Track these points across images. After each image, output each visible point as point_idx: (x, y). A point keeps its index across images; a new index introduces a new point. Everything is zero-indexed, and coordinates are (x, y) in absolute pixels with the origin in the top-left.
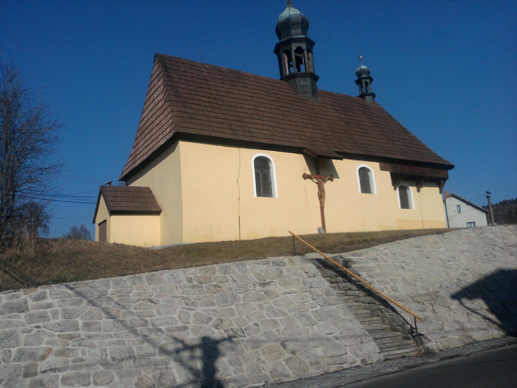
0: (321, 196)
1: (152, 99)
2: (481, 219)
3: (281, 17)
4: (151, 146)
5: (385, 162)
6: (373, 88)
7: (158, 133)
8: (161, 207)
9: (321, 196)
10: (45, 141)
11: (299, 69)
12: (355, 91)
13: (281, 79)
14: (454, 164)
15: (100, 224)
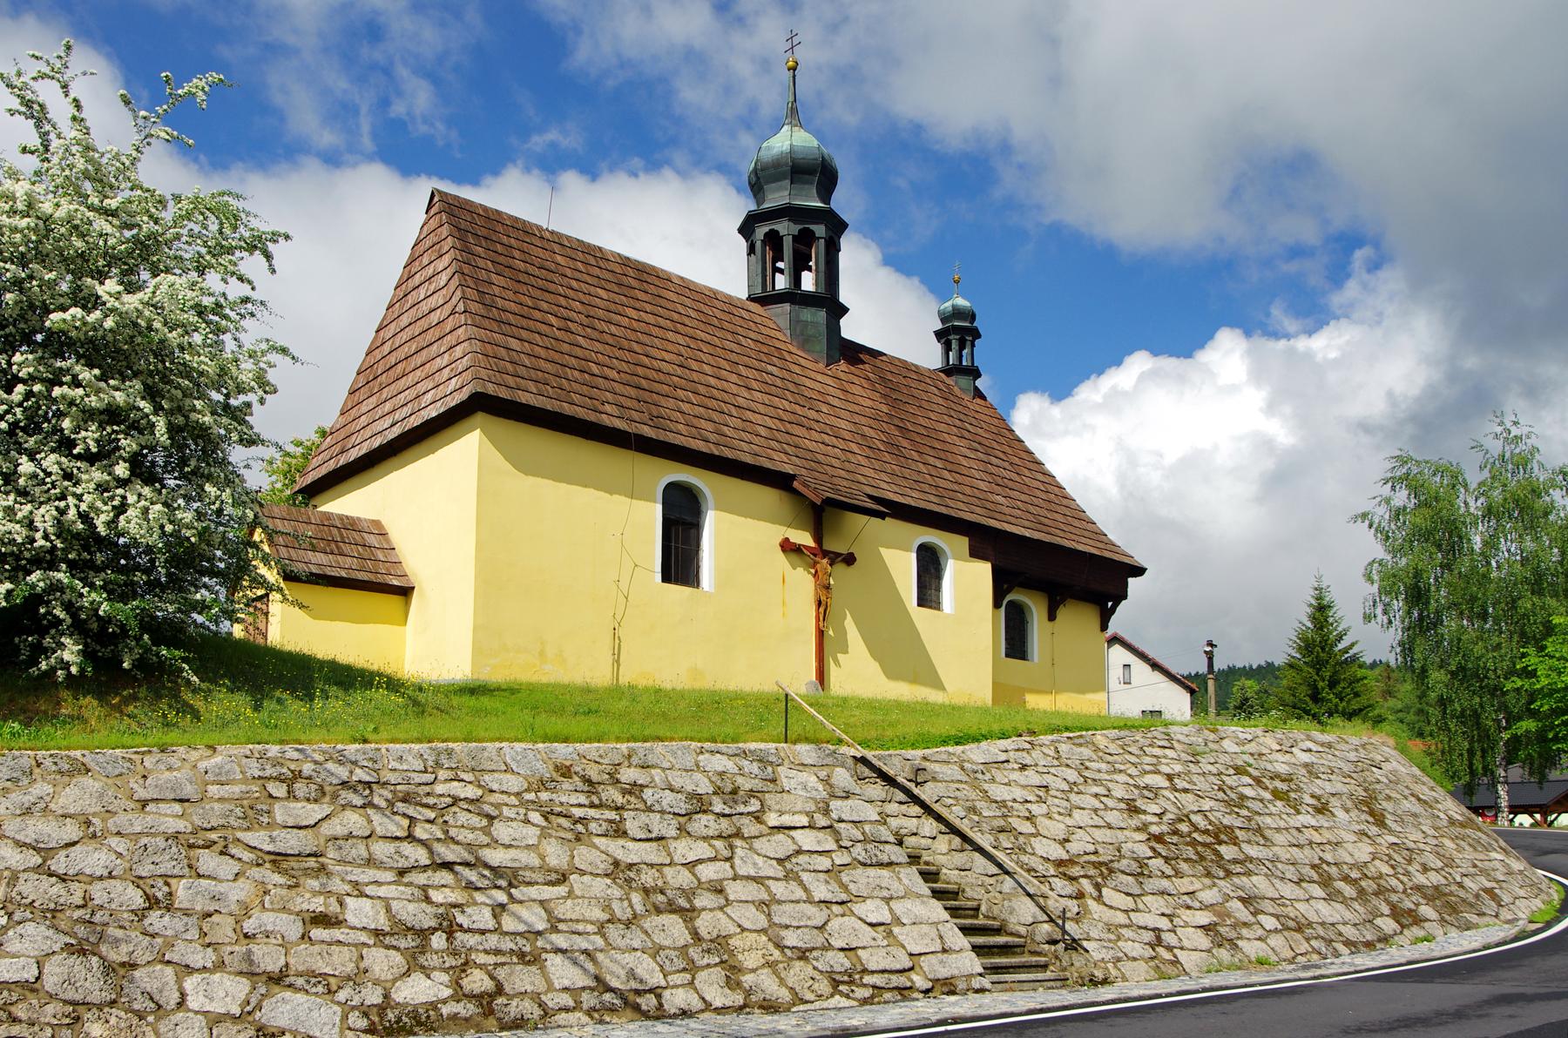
1: (411, 299)
2: (1177, 703)
3: (769, 148)
4: (398, 416)
5: (984, 542)
6: (983, 355)
7: (421, 387)
10: (1340, 638)
11: (797, 281)
12: (929, 356)
13: (750, 298)
14: (1140, 559)
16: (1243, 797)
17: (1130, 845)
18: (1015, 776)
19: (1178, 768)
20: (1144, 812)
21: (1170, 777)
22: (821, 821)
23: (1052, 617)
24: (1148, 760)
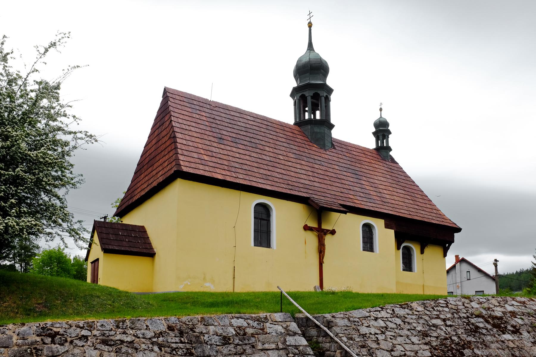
0: (310, 46)
5: (391, 220)
8: (155, 250)
9: (310, 46)
14: (460, 225)
15: (92, 263)
16: (477, 327)
17: (421, 351)
18: (373, 323)
19: (449, 316)
20: (431, 336)
21: (444, 320)
22: (281, 346)
23: (422, 252)
24: (435, 313)
